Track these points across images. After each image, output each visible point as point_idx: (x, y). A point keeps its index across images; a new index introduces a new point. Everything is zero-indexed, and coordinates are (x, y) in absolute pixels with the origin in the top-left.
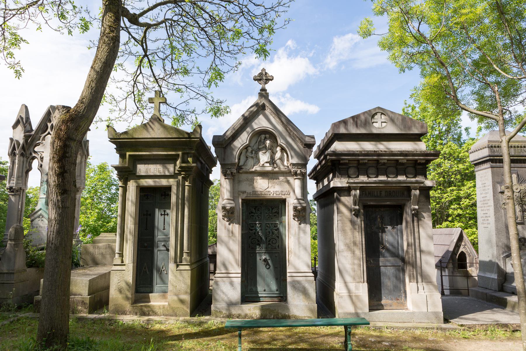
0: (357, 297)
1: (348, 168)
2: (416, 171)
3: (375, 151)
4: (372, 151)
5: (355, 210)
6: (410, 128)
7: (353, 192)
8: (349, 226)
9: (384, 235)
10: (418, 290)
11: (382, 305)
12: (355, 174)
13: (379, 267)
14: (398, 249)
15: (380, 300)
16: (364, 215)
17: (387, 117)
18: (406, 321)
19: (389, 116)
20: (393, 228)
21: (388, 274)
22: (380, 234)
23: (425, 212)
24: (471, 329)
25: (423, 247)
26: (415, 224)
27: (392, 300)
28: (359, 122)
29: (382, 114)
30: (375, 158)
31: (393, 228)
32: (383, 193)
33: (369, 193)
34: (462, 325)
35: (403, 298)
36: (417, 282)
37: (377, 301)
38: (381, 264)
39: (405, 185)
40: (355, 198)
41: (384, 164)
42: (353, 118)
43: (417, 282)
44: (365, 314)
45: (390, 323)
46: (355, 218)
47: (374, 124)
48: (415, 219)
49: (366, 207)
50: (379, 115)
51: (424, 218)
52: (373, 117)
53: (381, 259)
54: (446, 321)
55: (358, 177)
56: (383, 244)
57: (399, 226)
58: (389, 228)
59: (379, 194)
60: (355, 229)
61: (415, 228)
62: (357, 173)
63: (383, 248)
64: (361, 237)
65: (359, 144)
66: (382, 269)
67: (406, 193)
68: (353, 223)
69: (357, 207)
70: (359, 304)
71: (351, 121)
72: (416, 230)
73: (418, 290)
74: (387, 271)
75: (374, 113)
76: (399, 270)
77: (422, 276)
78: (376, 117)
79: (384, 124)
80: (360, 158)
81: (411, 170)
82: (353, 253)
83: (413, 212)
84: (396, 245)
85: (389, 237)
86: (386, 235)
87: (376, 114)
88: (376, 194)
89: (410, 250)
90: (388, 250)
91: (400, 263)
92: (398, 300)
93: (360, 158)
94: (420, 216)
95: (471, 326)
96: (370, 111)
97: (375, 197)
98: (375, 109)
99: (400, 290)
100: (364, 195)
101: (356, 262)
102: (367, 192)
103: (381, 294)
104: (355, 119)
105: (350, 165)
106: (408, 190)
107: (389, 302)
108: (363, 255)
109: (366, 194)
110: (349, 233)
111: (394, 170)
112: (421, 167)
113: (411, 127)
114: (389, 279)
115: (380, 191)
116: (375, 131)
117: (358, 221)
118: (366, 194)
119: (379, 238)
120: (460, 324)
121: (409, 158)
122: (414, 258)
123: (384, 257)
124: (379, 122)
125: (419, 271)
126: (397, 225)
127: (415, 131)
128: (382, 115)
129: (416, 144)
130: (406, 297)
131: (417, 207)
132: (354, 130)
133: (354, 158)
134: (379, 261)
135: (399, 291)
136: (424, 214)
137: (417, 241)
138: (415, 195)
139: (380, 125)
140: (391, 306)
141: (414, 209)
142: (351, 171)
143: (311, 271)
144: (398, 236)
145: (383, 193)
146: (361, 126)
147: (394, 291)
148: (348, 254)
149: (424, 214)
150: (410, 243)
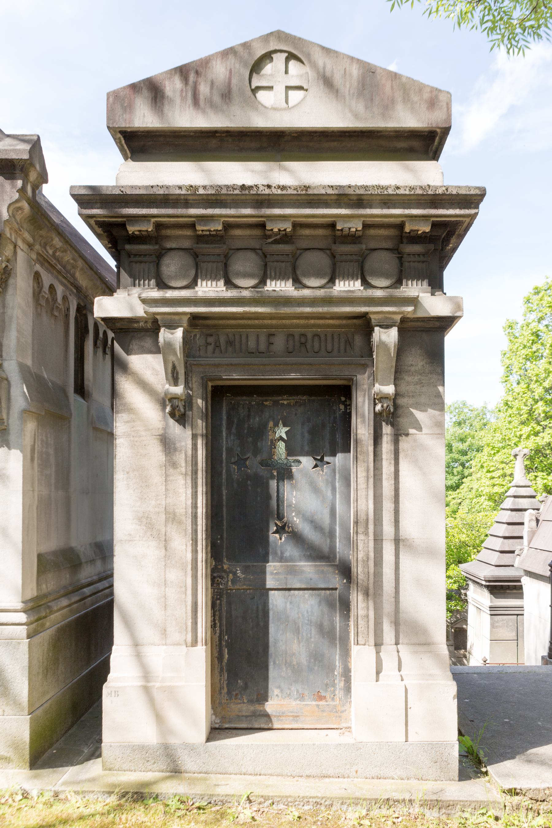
0: (171, 692)
1: (159, 256)
2: (401, 264)
3: (243, 187)
4: (234, 187)
5: (173, 399)
6: (387, 108)
7: (164, 335)
8: (156, 453)
9: (287, 489)
10: (378, 673)
11: (267, 716)
12: (184, 277)
13: (263, 592)
14: (332, 534)
15: (263, 697)
16: (205, 417)
17: (306, 69)
18: (331, 772)
19: (314, 65)
20: (320, 462)
21: (293, 614)
22: (273, 484)
23: (422, 407)
24: (543, 807)
25: (410, 527)
26: (386, 445)
27: (302, 698)
28: (204, 89)
29: (291, 56)
30: (248, 211)
31: (320, 462)
32: (279, 343)
33: (230, 343)
34: (513, 792)
35: (339, 693)
36: (378, 645)
37: (251, 702)
38: (270, 583)
39: (347, 309)
40: (172, 358)
41: (285, 238)
42: (183, 71)
43: (378, 645)
44: (191, 748)
45: (272, 780)
46: (175, 428)
47: (261, 95)
48: (387, 430)
49: (219, 394)
50: (279, 59)
51: (420, 429)
52: (256, 67)
53: (272, 567)
54: (472, 764)
55: (192, 285)
56: (280, 517)
57: (340, 456)
58: (307, 462)
59: (263, 347)
60: (174, 465)
61: (385, 463)
62: (193, 272)
63: (280, 530)
64: (189, 491)
65: (203, 170)
66: (276, 600)
67: (358, 340)
68: (167, 444)
69: (179, 390)
70: (175, 719)
71: (178, 83)
72: (387, 468)
73: (378, 673)
74: (292, 603)
75: (260, 52)
76: (331, 605)
77: (397, 623)
78: (268, 69)
79: (295, 96)
80: (193, 211)
81: (384, 260)
82: (166, 543)
83: (378, 407)
84: (326, 520)
85: (307, 493)
86: (294, 487)
87: (268, 57)
88: (252, 344)
89: (361, 537)
90: (296, 537)
91: (336, 581)
92: (321, 698)
93: (193, 211)
94: (403, 421)
95: (540, 797)
96: (246, 45)
97: (251, 353)
98: (266, 38)
99: (331, 669)
100: (210, 348)
101: (174, 575)
102: (222, 340)
103: (266, 678)
104: (192, 77)
105: (169, 245)
106: (364, 325)
107: (293, 704)
108: (195, 551)
109: (217, 346)
110: (157, 478)
111: (321, 260)
112: (417, 248)
113: (393, 101)
114: (297, 631)
115: (271, 335)
116: (260, 122)
117: (183, 436)
118: (217, 346)
119: (269, 497)
120: (507, 786)
121: (368, 211)
122: (371, 564)
123: (281, 559)
124: (280, 89)
125: (388, 607)
126: (334, 454)
127: (408, 119)
128: (292, 64)
129: (407, 168)
130: (348, 689)
131: (390, 389)
132: (185, 118)
133: (170, 211)
134: (264, 572)
135: (329, 671)
136: (418, 414)
137: (388, 506)
138: (382, 344)
139: (287, 102)
140: (296, 717)
141: (382, 398)
142: (171, 265)
143: (20, 606)
144: (334, 489)
145: (279, 343)
146: (212, 105)
147: (310, 669)
148: (150, 550)
149: (418, 414)
150: (362, 516)
